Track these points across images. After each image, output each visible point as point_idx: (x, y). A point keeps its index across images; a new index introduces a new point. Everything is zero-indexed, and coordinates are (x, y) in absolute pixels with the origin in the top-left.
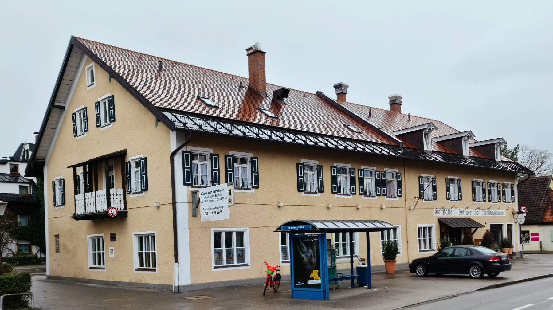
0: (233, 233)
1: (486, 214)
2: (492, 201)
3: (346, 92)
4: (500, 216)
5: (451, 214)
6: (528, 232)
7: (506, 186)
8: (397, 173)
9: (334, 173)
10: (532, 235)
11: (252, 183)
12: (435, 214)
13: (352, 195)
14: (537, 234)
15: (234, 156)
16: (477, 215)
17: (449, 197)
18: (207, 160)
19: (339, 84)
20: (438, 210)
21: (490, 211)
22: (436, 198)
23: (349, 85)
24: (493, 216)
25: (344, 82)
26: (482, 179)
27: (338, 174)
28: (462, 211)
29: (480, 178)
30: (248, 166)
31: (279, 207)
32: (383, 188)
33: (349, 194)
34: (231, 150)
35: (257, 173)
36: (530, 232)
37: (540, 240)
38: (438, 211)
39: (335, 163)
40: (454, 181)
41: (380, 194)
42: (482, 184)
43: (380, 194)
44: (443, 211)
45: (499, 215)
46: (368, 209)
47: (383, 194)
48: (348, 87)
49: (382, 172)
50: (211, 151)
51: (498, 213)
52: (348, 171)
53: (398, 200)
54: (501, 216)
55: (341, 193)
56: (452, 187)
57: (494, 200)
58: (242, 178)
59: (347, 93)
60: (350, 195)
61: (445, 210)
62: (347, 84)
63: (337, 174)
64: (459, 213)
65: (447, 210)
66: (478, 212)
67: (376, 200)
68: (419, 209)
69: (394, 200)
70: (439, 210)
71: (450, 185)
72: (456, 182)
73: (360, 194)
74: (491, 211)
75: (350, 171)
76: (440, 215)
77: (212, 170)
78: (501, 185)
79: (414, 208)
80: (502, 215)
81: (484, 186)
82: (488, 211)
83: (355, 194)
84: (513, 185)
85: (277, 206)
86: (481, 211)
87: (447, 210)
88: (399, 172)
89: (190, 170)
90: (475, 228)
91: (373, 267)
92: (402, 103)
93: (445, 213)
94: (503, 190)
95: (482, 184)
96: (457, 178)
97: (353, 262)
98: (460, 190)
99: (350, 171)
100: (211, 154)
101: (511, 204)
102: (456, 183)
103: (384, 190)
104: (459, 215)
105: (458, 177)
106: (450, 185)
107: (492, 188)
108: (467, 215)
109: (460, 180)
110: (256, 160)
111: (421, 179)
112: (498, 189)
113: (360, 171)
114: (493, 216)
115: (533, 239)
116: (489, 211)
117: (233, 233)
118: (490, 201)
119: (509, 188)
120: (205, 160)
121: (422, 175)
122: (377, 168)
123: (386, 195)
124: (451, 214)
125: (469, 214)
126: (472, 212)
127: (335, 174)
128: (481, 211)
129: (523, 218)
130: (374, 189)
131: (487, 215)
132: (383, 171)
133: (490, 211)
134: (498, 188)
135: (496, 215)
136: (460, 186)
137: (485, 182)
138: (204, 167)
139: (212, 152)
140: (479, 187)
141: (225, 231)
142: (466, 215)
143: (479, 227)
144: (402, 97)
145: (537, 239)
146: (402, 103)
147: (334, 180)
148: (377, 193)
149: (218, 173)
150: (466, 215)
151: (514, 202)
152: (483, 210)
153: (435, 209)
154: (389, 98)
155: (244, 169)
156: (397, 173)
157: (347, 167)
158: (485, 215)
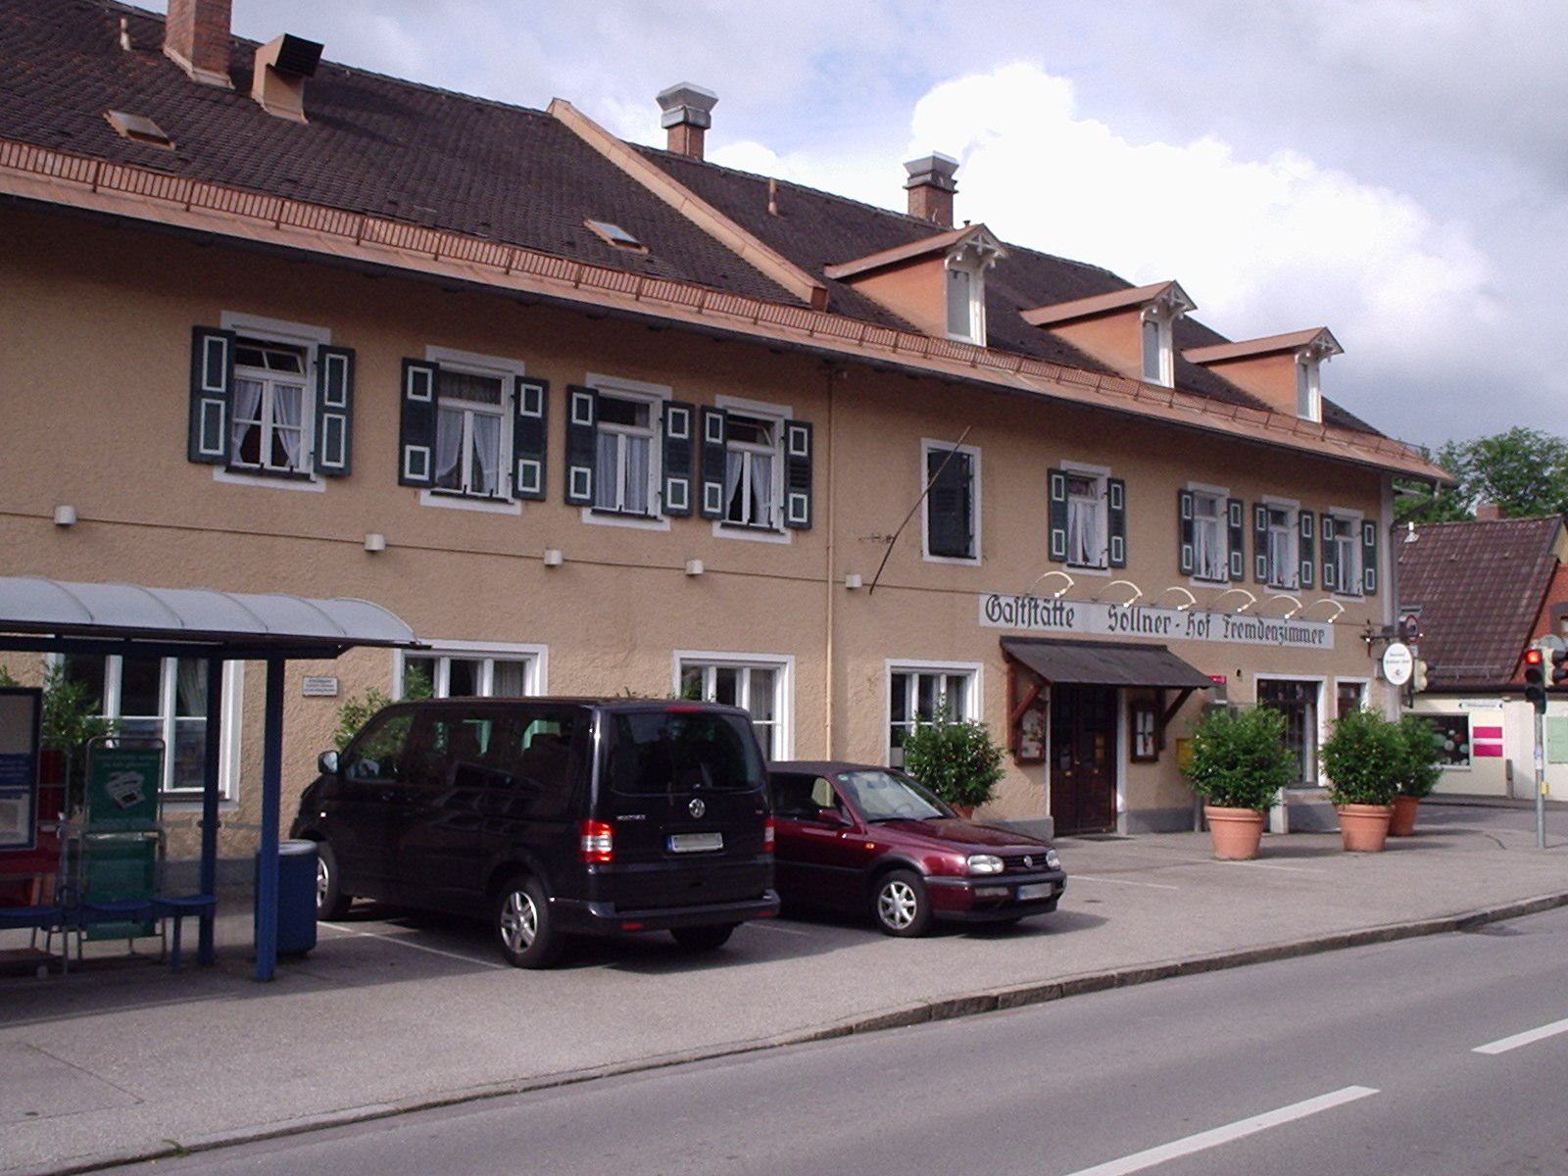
0: (938, 677)
1: (1243, 635)
2: (1341, 589)
3: (702, 122)
4: (1307, 645)
5: (1070, 626)
6: (1460, 722)
7: (1342, 527)
8: (786, 421)
9: (583, 416)
10: (1481, 732)
11: (316, 454)
12: (984, 621)
13: (518, 504)
14: (1496, 732)
15: (442, 364)
16: (1200, 638)
17: (1059, 549)
18: (502, 402)
19: (674, 90)
20: (1003, 601)
21: (1261, 623)
22: (1121, 560)
23: (718, 95)
24: (1276, 643)
25: (701, 84)
26: (1297, 498)
27: (443, 402)
28: (1124, 615)
29: (1218, 483)
30: (307, 384)
31: (692, 576)
32: (708, 485)
33: (775, 526)
34: (1193, 479)
35: (349, 411)
36: (1472, 724)
37: (1506, 755)
38: (1003, 605)
39: (224, 312)
40: (1091, 485)
41: (685, 506)
42: (1363, 529)
43: (685, 506)
44: (1026, 610)
45: (1299, 644)
46: (613, 572)
47: (707, 509)
48: (713, 101)
49: (704, 410)
50: (324, 335)
51: (1299, 634)
52: (507, 390)
53: (979, 564)
54: (1311, 645)
55: (741, 520)
56: (1078, 507)
57: (1211, 569)
58: (275, 430)
59: (708, 127)
60: (782, 529)
61: (1036, 606)
62: (713, 93)
63: (725, 442)
64: (1113, 622)
65: (1051, 606)
66: (1201, 622)
67: (663, 533)
68: (897, 593)
69: (766, 543)
70: (1008, 605)
71: (1066, 500)
72: (1102, 486)
73: (569, 501)
74: (1268, 622)
75: (665, 413)
76: (1047, 628)
77: (321, 408)
78: (1317, 520)
79: (874, 585)
80: (1317, 645)
81: (1117, 498)
82: (1252, 623)
83: (539, 498)
84: (1373, 523)
85: (360, 547)
86: (1217, 621)
87: (1051, 606)
88: (799, 418)
89: (343, 418)
90: (1180, 691)
91: (227, 863)
92: (956, 187)
93: (1039, 619)
94: (1323, 541)
95: (1363, 529)
96: (1106, 472)
97: (200, 824)
98: (1117, 525)
99: (665, 413)
100: (664, 402)
101: (1363, 600)
102: (1099, 494)
103: (713, 491)
104: (1110, 632)
105: (670, 389)
106: (1070, 498)
107: (1275, 529)
108: (1148, 634)
109: (1122, 483)
110: (540, 389)
111: (1187, 500)
112: (1109, 505)
113: (576, 395)
114: (1276, 643)
115: (1482, 751)
116: (1257, 624)
117: (911, 676)
118: (1265, 582)
119: (1354, 534)
120: (496, 401)
121: (1191, 486)
122: (674, 390)
123: (590, 503)
124: (1070, 626)
125: (1161, 629)
126: (1173, 625)
127: (428, 399)
128: (1217, 621)
129: (1404, 662)
130: (654, 485)
131: (1244, 640)
132: (213, 325)
133: (1261, 623)
134: (1109, 500)
135: (1286, 643)
136: (1371, 544)
137: (1240, 502)
138: (637, 443)
139: (669, 397)
140: (1212, 519)
141: (949, 672)
142: (1141, 634)
143: (1196, 688)
144: (957, 166)
145: (1495, 751)
146: (956, 187)
147: (418, 424)
148: (670, 505)
149: (331, 416)
150: (1141, 634)
151: (1373, 593)
152: (1229, 616)
153: (983, 599)
154: (908, 165)
155: (485, 421)
156: (786, 421)
157: (500, 374)
158: (1237, 639)
